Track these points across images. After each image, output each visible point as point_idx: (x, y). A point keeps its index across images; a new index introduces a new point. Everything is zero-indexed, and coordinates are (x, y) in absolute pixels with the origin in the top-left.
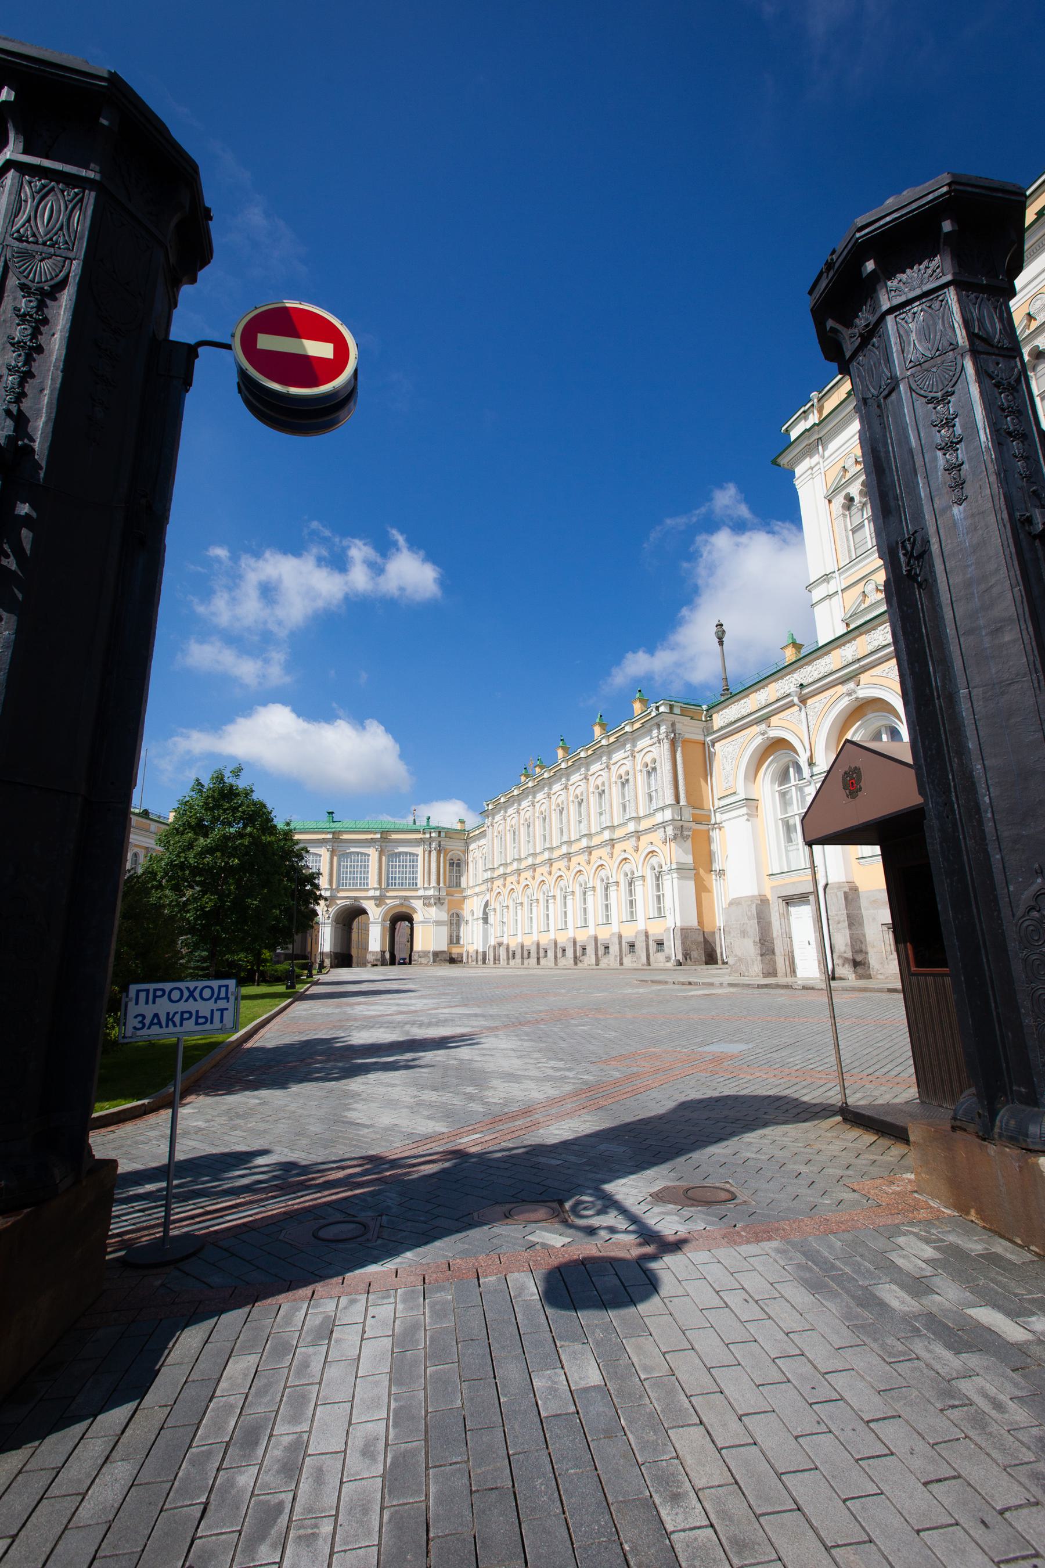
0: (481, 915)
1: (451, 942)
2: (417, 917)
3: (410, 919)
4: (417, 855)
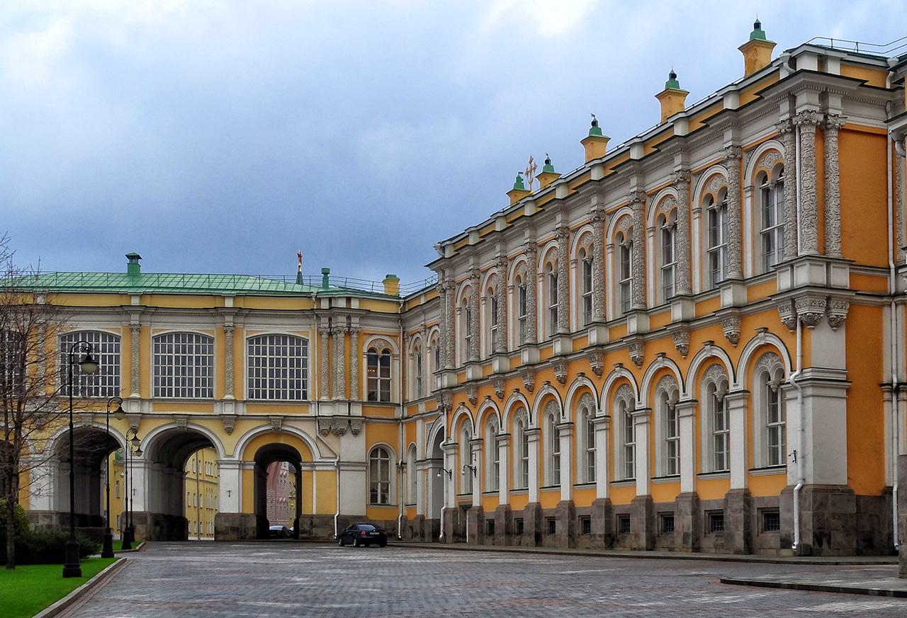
0: (430, 454)
1: (373, 498)
2: (316, 451)
3: (292, 456)
4: (305, 342)
